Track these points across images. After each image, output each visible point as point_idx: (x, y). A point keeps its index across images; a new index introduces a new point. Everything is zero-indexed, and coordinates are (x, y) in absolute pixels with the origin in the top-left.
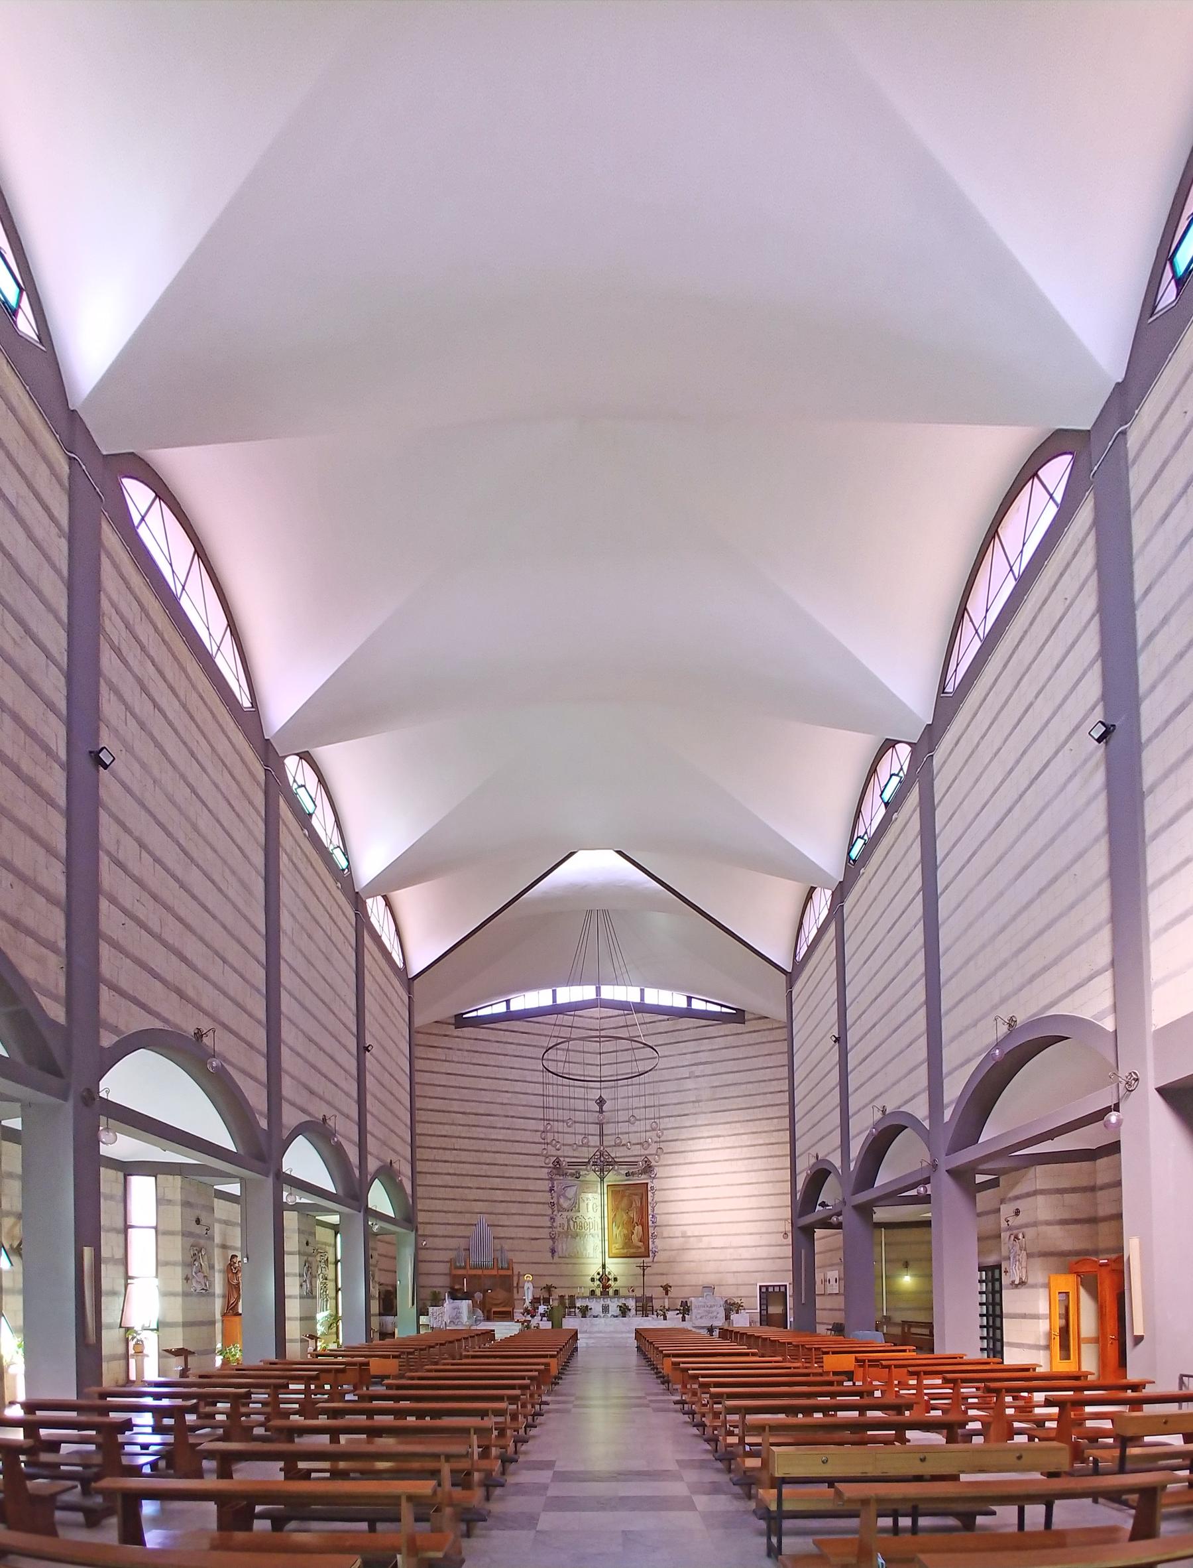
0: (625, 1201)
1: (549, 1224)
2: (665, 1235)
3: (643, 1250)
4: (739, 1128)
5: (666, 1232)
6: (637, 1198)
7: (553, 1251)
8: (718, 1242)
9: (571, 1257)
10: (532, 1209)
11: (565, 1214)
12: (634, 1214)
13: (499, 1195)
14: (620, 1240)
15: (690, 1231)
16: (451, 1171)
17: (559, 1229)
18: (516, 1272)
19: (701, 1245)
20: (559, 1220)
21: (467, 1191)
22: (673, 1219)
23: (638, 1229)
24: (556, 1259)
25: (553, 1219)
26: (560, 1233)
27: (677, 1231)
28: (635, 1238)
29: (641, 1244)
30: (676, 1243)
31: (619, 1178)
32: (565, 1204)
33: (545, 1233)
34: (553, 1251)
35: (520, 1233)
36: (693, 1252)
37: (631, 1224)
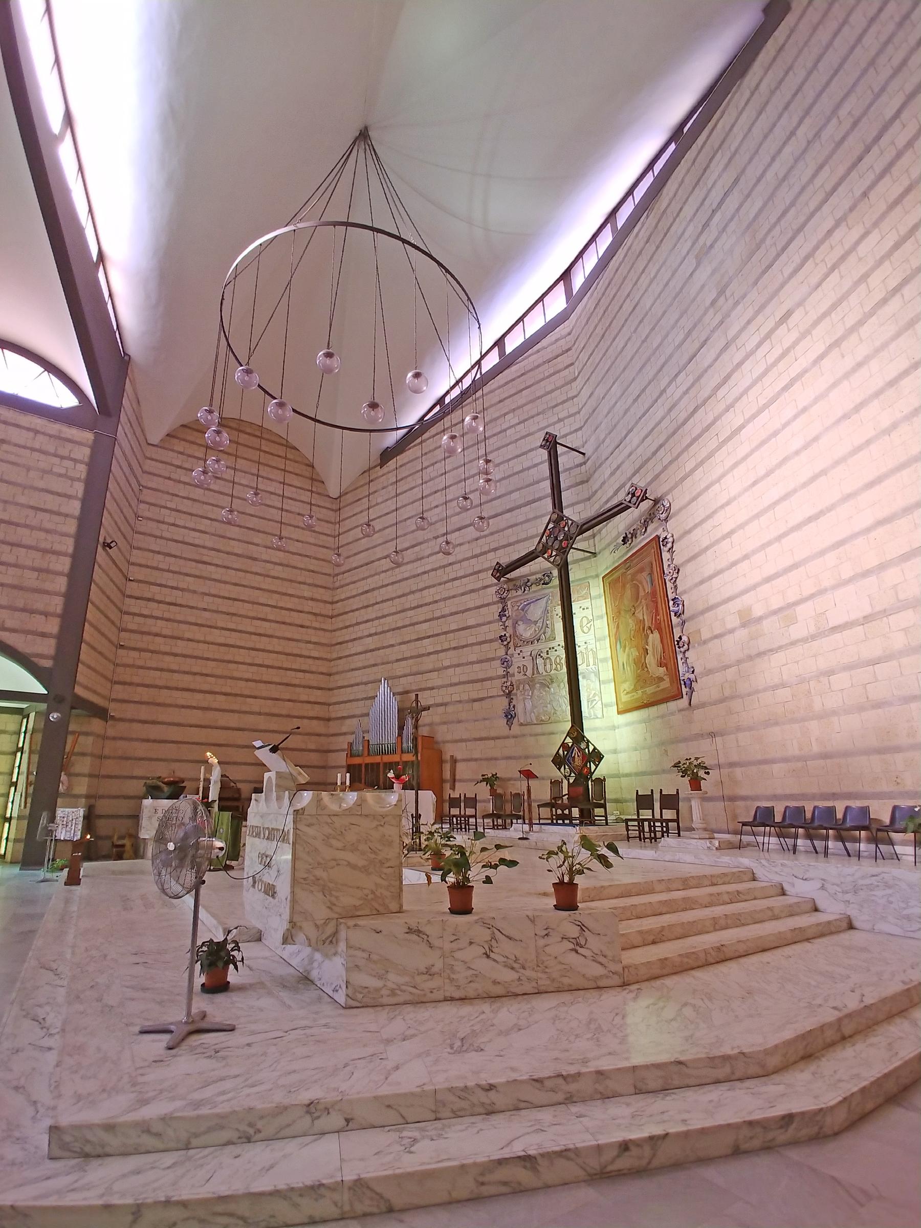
0: (628, 593)
1: (501, 671)
2: (705, 635)
3: (666, 684)
4: (846, 236)
5: (705, 627)
6: (644, 577)
7: (510, 716)
8: (848, 604)
9: (542, 723)
10: (472, 655)
11: (527, 650)
12: (643, 614)
13: (428, 645)
14: (629, 672)
15: (757, 604)
16: (373, 631)
17: (519, 677)
18: (447, 757)
19: (798, 631)
20: (517, 662)
21: (388, 651)
22: (718, 589)
23: (654, 637)
24: (516, 729)
25: (506, 662)
26: (520, 682)
27: (729, 616)
28: (651, 660)
29: (662, 670)
30: (731, 646)
31: (618, 554)
32: (526, 632)
33: (495, 687)
34: (510, 716)
35: (457, 693)
36: (779, 658)
37: (642, 631)
